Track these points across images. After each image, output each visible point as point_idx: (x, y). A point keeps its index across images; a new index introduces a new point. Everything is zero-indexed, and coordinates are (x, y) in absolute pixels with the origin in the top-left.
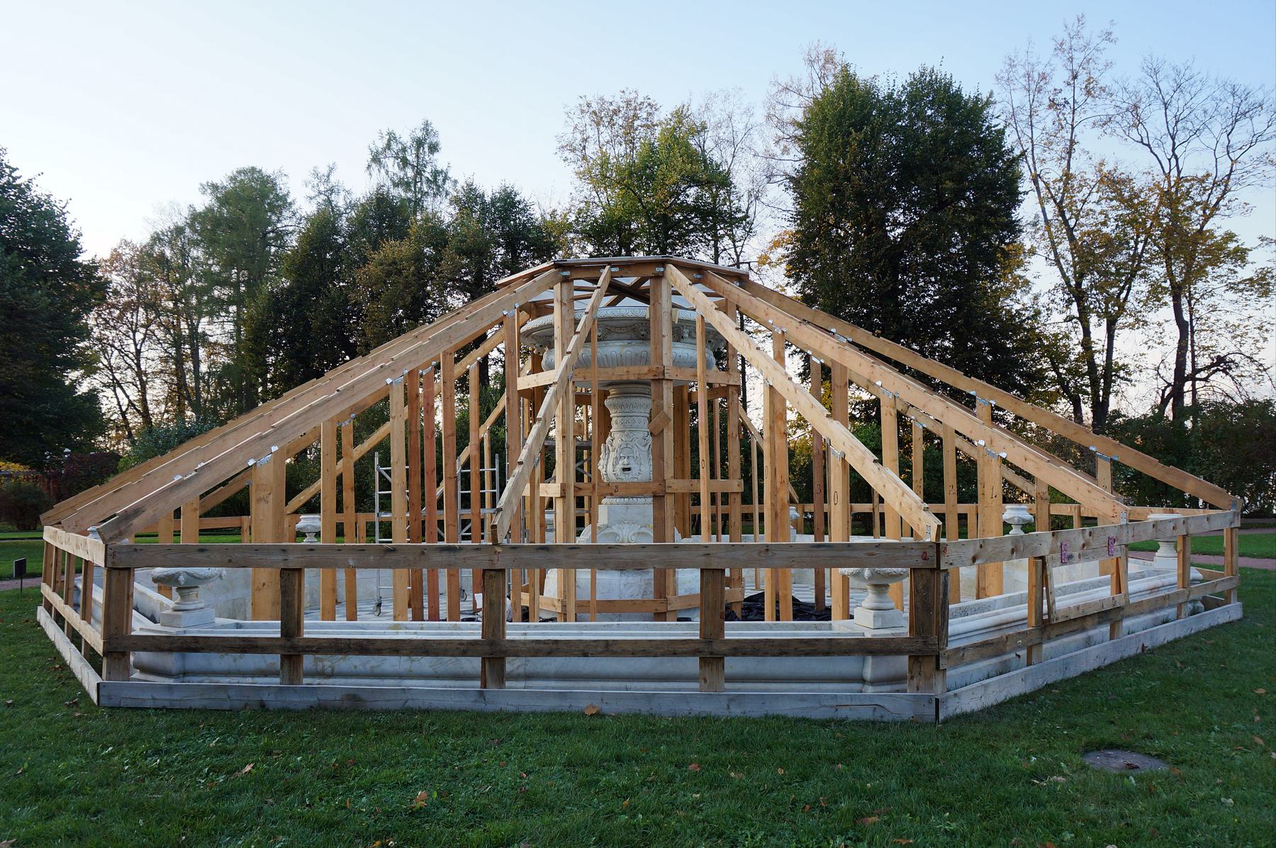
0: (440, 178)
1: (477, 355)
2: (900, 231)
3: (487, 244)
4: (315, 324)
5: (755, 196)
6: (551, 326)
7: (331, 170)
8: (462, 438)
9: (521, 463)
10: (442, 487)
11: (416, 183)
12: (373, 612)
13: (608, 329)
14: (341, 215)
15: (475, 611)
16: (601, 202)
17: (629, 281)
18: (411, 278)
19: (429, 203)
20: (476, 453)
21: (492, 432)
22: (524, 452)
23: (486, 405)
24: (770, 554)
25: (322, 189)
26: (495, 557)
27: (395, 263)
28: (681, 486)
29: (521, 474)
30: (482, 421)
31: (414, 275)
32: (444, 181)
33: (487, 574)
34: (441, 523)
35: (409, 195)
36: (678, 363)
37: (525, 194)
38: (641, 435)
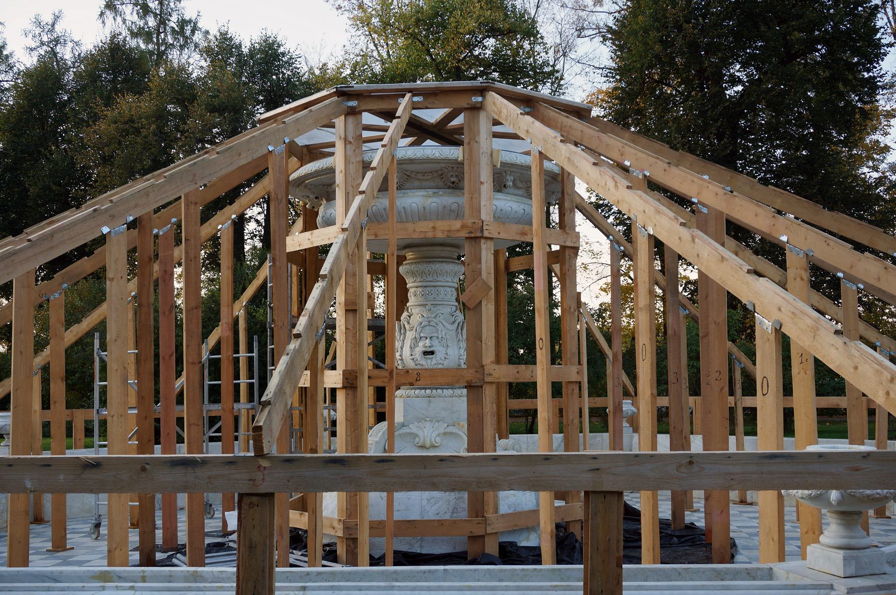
0: (188, 30)
1: (231, 213)
2: (740, 88)
3: (244, 101)
4: (33, 191)
5: (564, 50)
6: (331, 171)
7: (57, 18)
8: (210, 315)
9: (298, 336)
10: (183, 379)
11: (159, 33)
12: (89, 534)
13: (409, 175)
14: (68, 70)
15: (226, 533)
16: (380, 53)
17: (432, 115)
18: (152, 139)
19: (174, 55)
20: (229, 334)
21: (250, 316)
22: (303, 321)
23: (240, 283)
24: (695, 468)
25: (45, 39)
26: (259, 476)
27: (132, 121)
28: (507, 373)
29: (297, 351)
30: (236, 297)
31: (154, 134)
32: (193, 32)
33: (246, 500)
34: (180, 421)
35: (150, 47)
36: (500, 218)
37: (289, 44)
38: (447, 310)
